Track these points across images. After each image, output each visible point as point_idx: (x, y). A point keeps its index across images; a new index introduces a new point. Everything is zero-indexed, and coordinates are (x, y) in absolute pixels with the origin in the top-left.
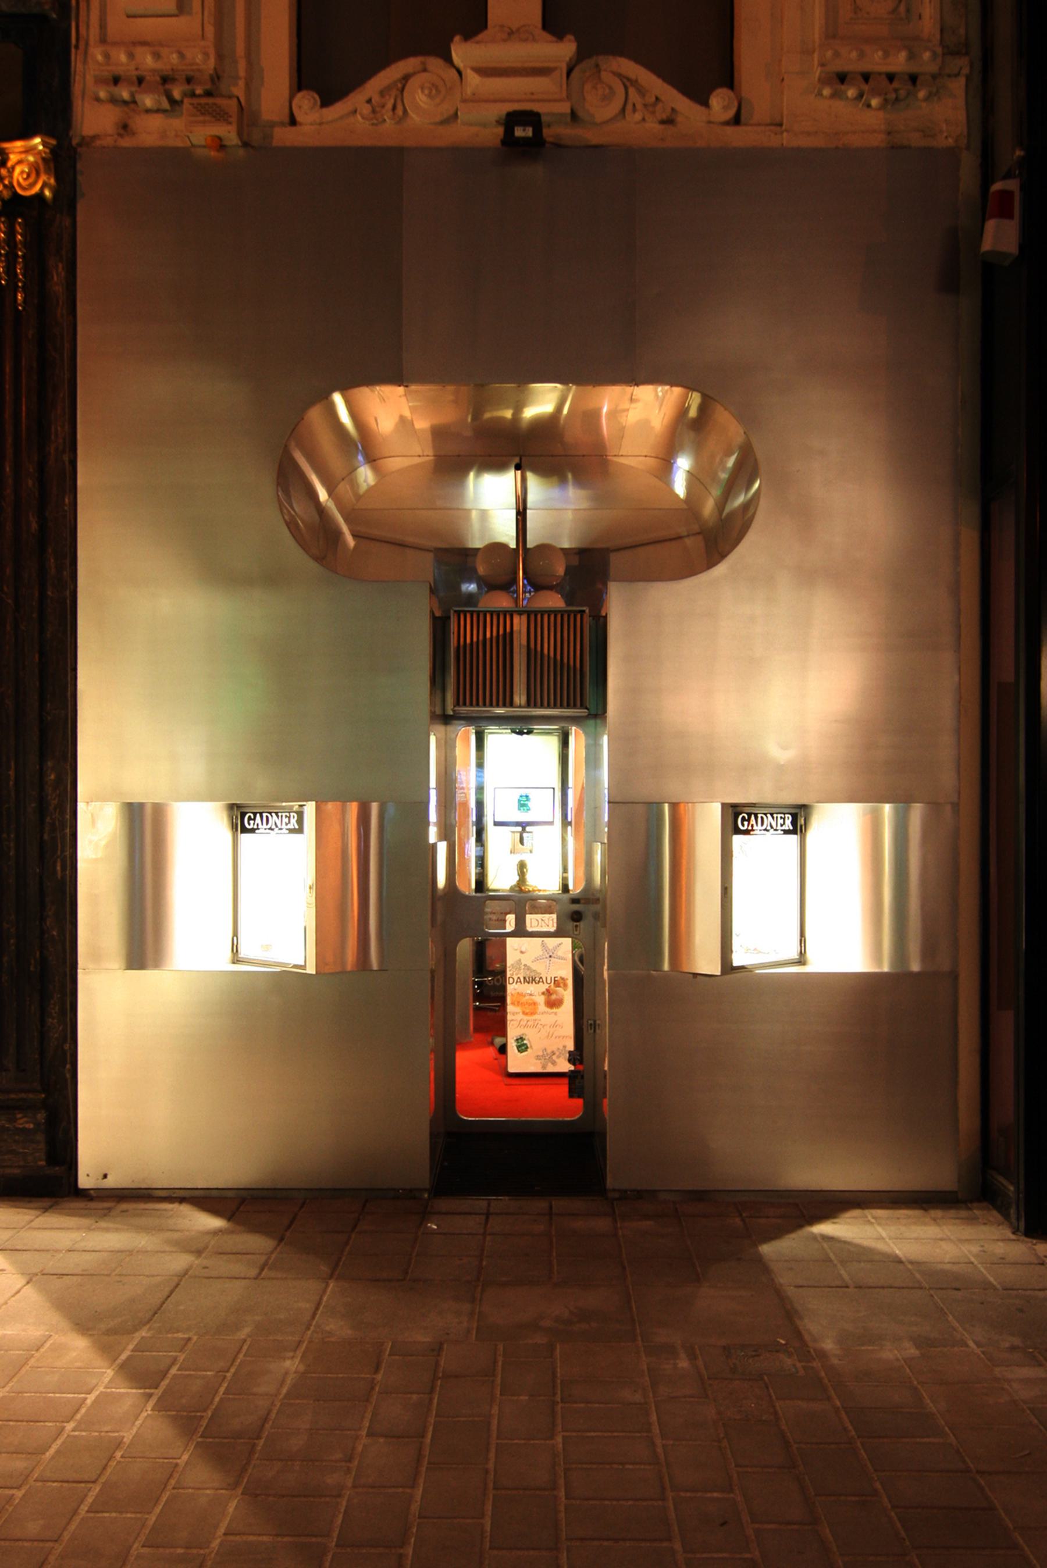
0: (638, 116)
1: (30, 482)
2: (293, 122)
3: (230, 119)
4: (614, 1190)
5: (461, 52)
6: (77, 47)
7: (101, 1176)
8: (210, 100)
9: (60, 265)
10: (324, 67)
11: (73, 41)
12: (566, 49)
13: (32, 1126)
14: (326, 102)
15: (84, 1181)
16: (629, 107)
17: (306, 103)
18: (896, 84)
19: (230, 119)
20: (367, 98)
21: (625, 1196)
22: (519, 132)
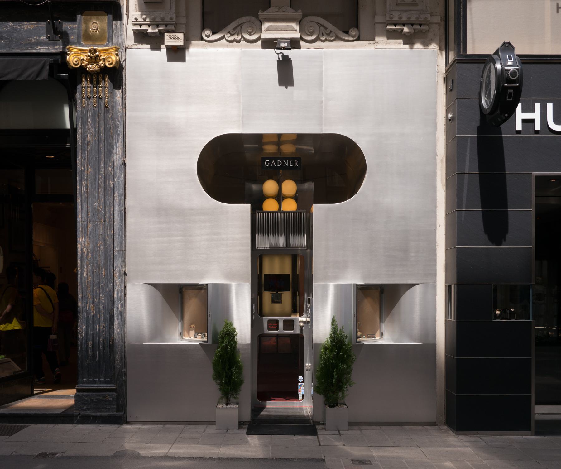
16: (321, 33)
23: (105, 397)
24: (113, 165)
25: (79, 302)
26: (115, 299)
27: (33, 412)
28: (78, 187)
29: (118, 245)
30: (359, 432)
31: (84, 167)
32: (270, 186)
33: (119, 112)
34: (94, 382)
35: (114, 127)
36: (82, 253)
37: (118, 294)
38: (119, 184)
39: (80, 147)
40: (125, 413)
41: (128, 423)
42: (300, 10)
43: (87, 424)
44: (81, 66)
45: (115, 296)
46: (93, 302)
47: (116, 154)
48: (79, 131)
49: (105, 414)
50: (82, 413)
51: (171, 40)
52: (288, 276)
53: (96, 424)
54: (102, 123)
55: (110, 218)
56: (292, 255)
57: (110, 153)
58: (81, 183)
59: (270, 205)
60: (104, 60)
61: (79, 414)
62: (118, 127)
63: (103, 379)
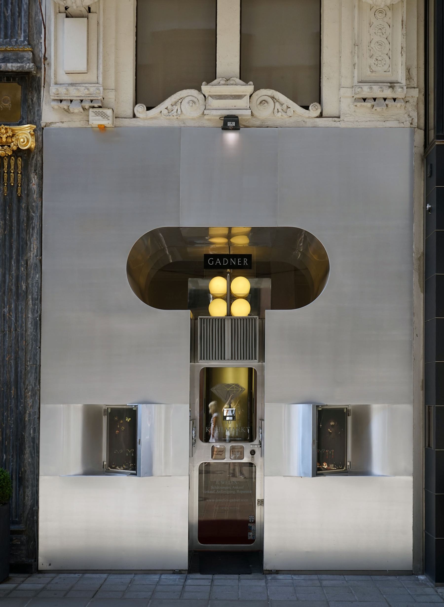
0: (280, 114)
1: (22, 268)
2: (134, 116)
3: (109, 118)
4: (266, 570)
5: (205, 88)
6: (44, 87)
7: (48, 565)
8: (100, 110)
9: (36, 177)
10: (147, 94)
11: (43, 85)
12: (250, 88)
13: (19, 543)
14: (148, 109)
15: (41, 567)
16: (276, 110)
17: (140, 109)
18: (387, 102)
19: (109, 118)
20: (166, 107)
21: (270, 572)
22: (229, 124)
24: (27, 264)
26: (27, 423)
27: (421, 393)
29: (30, 359)
32: (218, 285)
33: (34, 202)
35: (29, 219)
38: (32, 286)
40: (35, 561)
42: (251, 83)
45: (26, 419)
47: (30, 251)
51: (97, 118)
54: (14, 214)
56: (249, 368)
57: (23, 248)
59: (217, 309)
62: (32, 219)
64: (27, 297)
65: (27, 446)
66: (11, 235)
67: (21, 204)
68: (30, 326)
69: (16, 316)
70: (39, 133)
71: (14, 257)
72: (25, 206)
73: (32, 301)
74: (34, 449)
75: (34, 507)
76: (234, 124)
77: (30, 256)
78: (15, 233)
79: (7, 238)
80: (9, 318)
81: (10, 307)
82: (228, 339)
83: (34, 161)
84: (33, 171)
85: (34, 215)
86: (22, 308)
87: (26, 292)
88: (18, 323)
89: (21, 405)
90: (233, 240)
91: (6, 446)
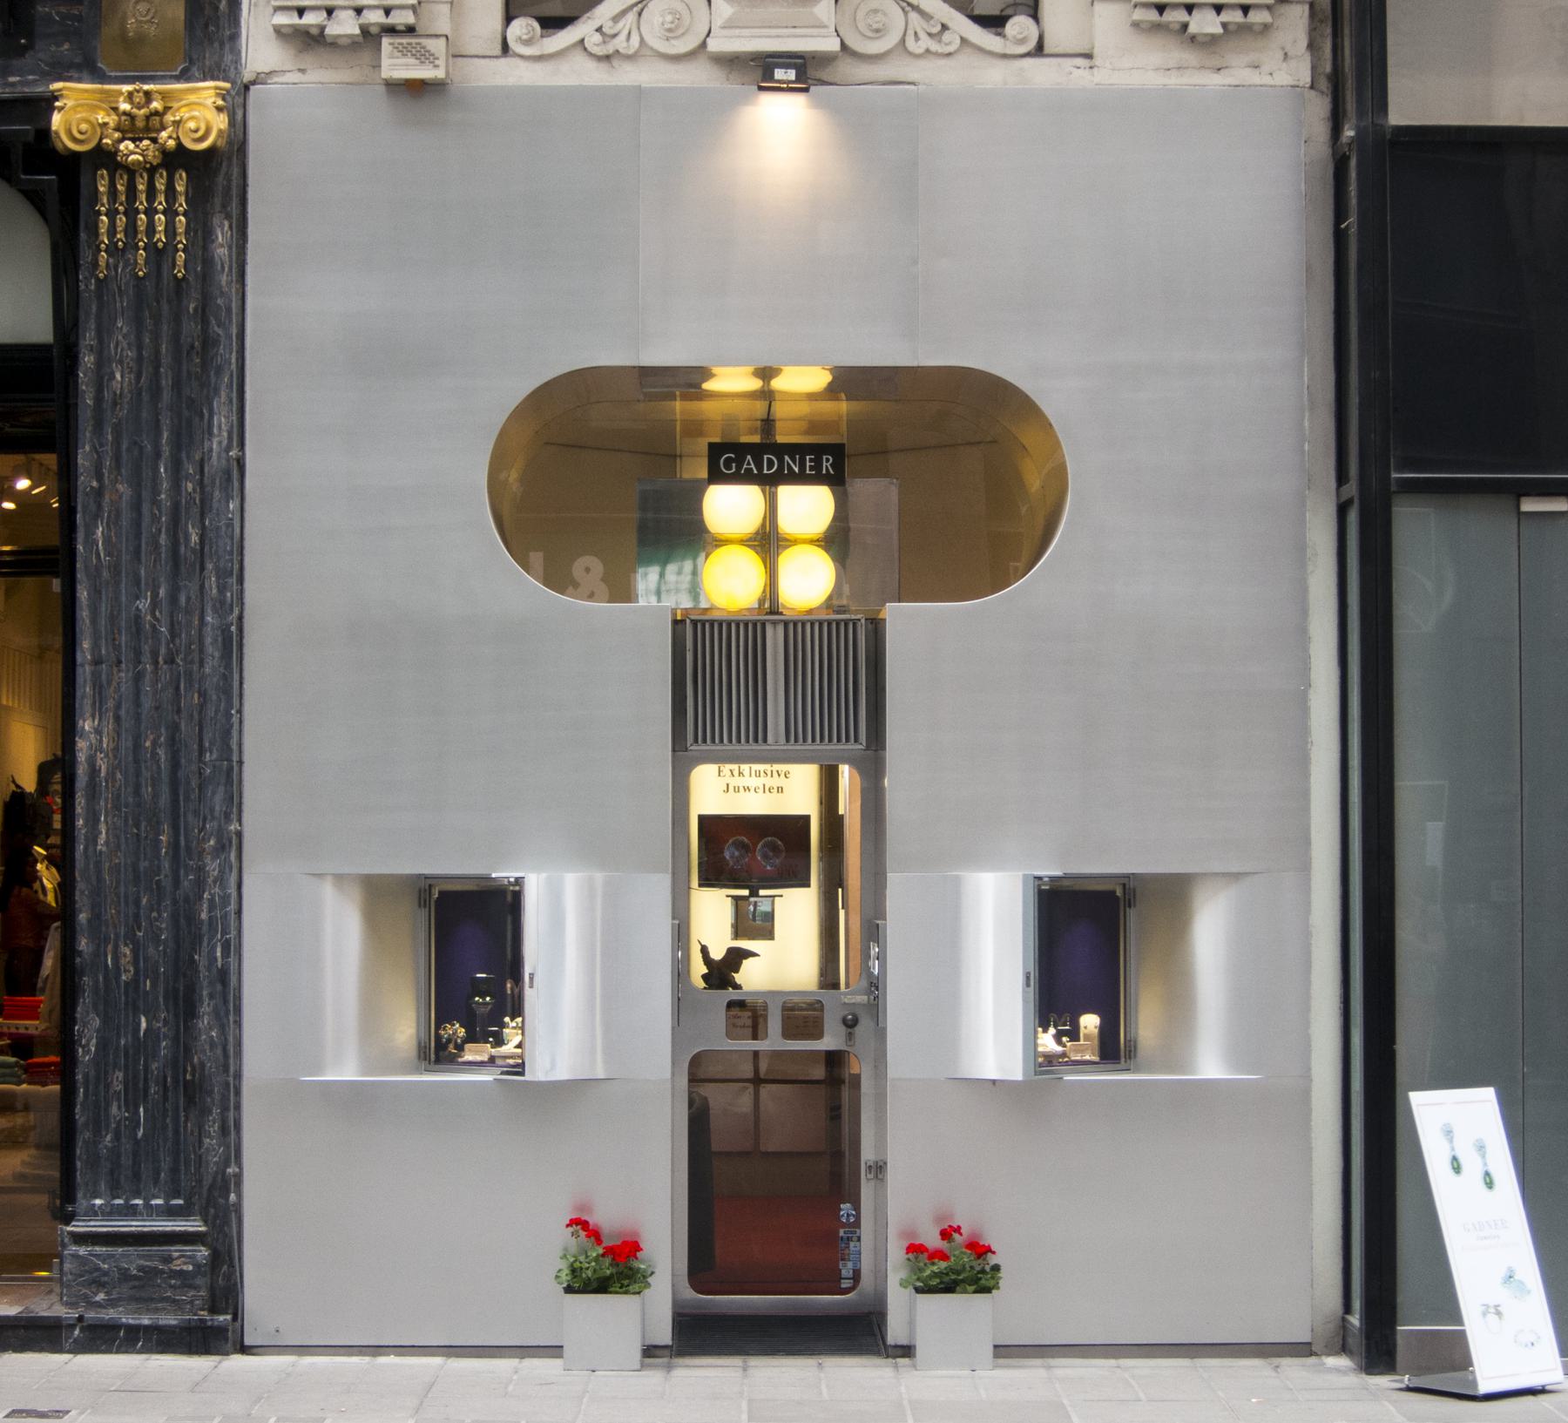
1: (190, 485)
2: (505, 48)
9: (226, 223)
13: (191, 1268)
16: (910, 32)
23: (168, 1260)
25: (78, 937)
28: (80, 547)
30: (1042, 1372)
31: (99, 477)
34: (131, 1212)
36: (93, 771)
37: (211, 908)
39: (89, 413)
41: (244, 1349)
43: (108, 1351)
44: (99, 145)
45: (204, 916)
46: (131, 938)
47: (211, 434)
48: (88, 360)
49: (170, 1320)
50: (91, 1315)
52: (807, 819)
53: (140, 1352)
55: (189, 651)
57: (189, 428)
58: (90, 533)
60: (177, 124)
61: (81, 1319)
62: (216, 342)
63: (159, 1202)
64: (202, 568)
65: (205, 993)
66: (156, 391)
67: (185, 302)
68: (210, 649)
69: (172, 624)
70: (237, 101)
71: (166, 450)
72: (196, 309)
73: (218, 578)
74: (226, 1002)
75: (227, 1165)
76: (791, 75)
77: (211, 450)
78: (166, 382)
79: (146, 397)
80: (153, 627)
81: (155, 595)
82: (776, 683)
83: (220, 179)
84: (218, 207)
85: (220, 332)
86: (188, 599)
87: (201, 553)
88: (177, 641)
89: (187, 875)
90: (778, 384)
91: (146, 993)
